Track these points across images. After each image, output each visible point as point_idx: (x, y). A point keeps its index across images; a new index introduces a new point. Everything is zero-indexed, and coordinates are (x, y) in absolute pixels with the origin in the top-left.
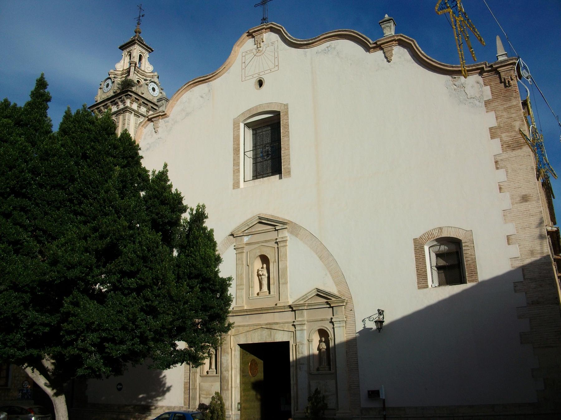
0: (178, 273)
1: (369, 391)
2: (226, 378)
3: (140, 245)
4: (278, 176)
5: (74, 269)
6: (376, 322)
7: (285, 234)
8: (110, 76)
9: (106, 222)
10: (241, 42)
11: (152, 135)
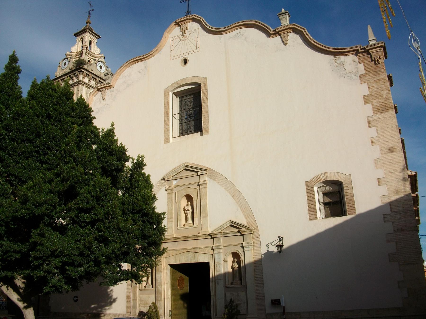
0: (123, 209)
1: (272, 300)
2: (160, 291)
3: (94, 187)
4: (199, 133)
5: (41, 207)
6: (277, 246)
7: (205, 178)
8: (67, 57)
9: (66, 169)
10: (170, 29)
11: (101, 102)
